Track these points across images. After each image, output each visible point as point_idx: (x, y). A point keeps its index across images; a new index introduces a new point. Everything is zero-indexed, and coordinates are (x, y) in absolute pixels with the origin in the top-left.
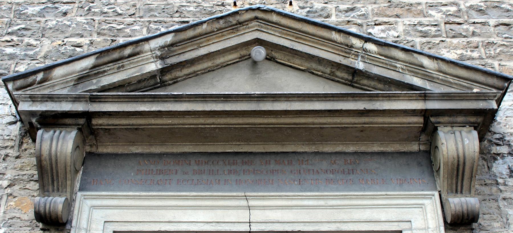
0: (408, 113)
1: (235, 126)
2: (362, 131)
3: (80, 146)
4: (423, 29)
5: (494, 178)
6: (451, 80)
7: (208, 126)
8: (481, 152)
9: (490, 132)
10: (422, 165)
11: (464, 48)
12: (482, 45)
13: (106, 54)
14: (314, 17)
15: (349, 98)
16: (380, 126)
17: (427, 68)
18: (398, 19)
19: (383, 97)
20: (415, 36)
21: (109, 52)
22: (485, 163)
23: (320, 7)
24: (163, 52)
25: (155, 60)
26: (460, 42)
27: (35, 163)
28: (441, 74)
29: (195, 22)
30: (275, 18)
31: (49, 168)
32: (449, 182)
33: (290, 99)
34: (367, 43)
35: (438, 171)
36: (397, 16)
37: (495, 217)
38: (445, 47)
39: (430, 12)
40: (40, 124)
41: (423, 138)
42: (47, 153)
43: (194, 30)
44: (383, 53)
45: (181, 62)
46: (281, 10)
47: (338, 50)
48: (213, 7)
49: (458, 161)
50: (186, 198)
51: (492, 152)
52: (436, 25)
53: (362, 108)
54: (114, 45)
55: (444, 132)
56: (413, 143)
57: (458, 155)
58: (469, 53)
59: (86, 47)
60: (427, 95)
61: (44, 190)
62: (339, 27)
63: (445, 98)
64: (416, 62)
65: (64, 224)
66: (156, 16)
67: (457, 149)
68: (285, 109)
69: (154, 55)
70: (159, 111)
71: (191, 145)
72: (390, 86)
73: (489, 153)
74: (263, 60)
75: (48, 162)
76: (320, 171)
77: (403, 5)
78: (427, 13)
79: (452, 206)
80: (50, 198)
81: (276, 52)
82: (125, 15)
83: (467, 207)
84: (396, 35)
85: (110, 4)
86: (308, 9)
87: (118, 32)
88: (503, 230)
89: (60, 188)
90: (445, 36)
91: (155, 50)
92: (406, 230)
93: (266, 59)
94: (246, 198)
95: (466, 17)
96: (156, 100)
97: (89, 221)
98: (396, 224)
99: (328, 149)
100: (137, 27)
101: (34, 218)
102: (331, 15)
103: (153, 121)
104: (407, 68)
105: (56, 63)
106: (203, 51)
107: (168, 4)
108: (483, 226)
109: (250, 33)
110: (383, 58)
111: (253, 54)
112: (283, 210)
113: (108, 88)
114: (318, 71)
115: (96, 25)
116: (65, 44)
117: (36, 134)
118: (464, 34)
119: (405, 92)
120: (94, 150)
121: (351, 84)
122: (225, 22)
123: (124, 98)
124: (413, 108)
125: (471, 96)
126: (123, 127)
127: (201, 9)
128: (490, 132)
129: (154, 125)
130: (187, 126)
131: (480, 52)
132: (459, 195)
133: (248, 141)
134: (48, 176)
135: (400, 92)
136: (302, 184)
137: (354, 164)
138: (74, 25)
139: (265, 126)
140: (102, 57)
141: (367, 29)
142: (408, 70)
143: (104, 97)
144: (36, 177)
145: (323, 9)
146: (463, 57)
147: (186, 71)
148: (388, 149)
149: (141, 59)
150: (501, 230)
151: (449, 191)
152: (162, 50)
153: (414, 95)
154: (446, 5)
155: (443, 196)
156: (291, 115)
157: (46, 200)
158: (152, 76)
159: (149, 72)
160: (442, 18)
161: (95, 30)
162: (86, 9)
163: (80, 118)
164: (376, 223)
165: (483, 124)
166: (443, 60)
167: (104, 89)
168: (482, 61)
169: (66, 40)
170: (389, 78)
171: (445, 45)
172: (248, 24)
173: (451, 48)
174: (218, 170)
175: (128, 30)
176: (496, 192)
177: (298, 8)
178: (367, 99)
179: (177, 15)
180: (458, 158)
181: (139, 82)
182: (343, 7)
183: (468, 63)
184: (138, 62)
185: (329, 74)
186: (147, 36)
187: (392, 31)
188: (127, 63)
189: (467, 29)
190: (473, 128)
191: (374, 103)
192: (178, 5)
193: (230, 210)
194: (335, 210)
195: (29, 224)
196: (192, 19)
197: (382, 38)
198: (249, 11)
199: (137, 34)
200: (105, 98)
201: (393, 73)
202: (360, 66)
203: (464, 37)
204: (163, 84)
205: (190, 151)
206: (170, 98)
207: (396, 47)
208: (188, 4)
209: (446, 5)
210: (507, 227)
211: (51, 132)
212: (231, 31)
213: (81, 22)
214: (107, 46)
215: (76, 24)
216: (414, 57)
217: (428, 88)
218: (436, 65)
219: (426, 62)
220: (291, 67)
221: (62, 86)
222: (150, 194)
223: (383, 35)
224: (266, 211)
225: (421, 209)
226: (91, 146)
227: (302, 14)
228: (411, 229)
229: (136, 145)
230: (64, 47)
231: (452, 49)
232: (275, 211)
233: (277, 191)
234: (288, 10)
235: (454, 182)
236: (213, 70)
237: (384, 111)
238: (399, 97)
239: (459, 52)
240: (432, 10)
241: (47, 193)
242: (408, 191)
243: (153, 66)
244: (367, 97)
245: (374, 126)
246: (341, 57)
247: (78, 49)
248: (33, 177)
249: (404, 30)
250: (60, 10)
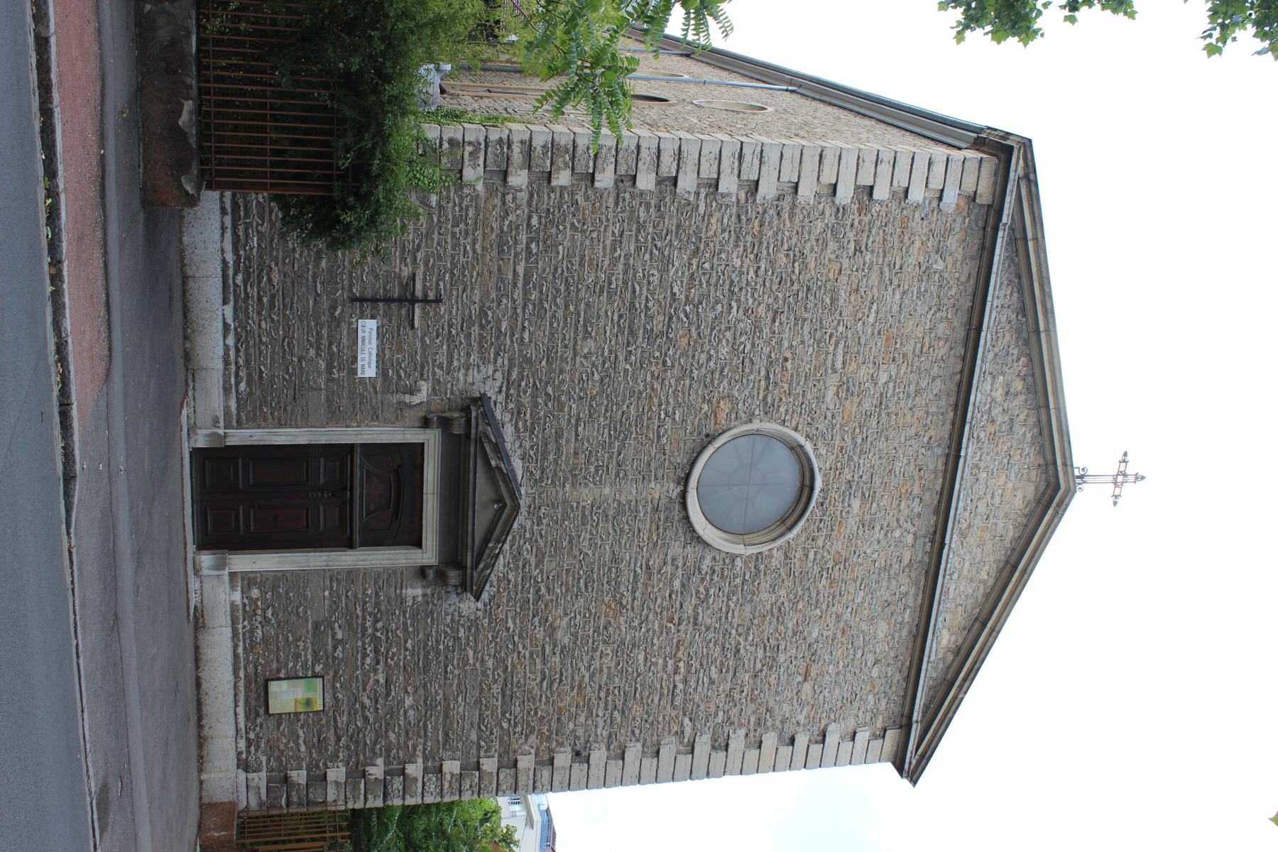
243: (493, 463)
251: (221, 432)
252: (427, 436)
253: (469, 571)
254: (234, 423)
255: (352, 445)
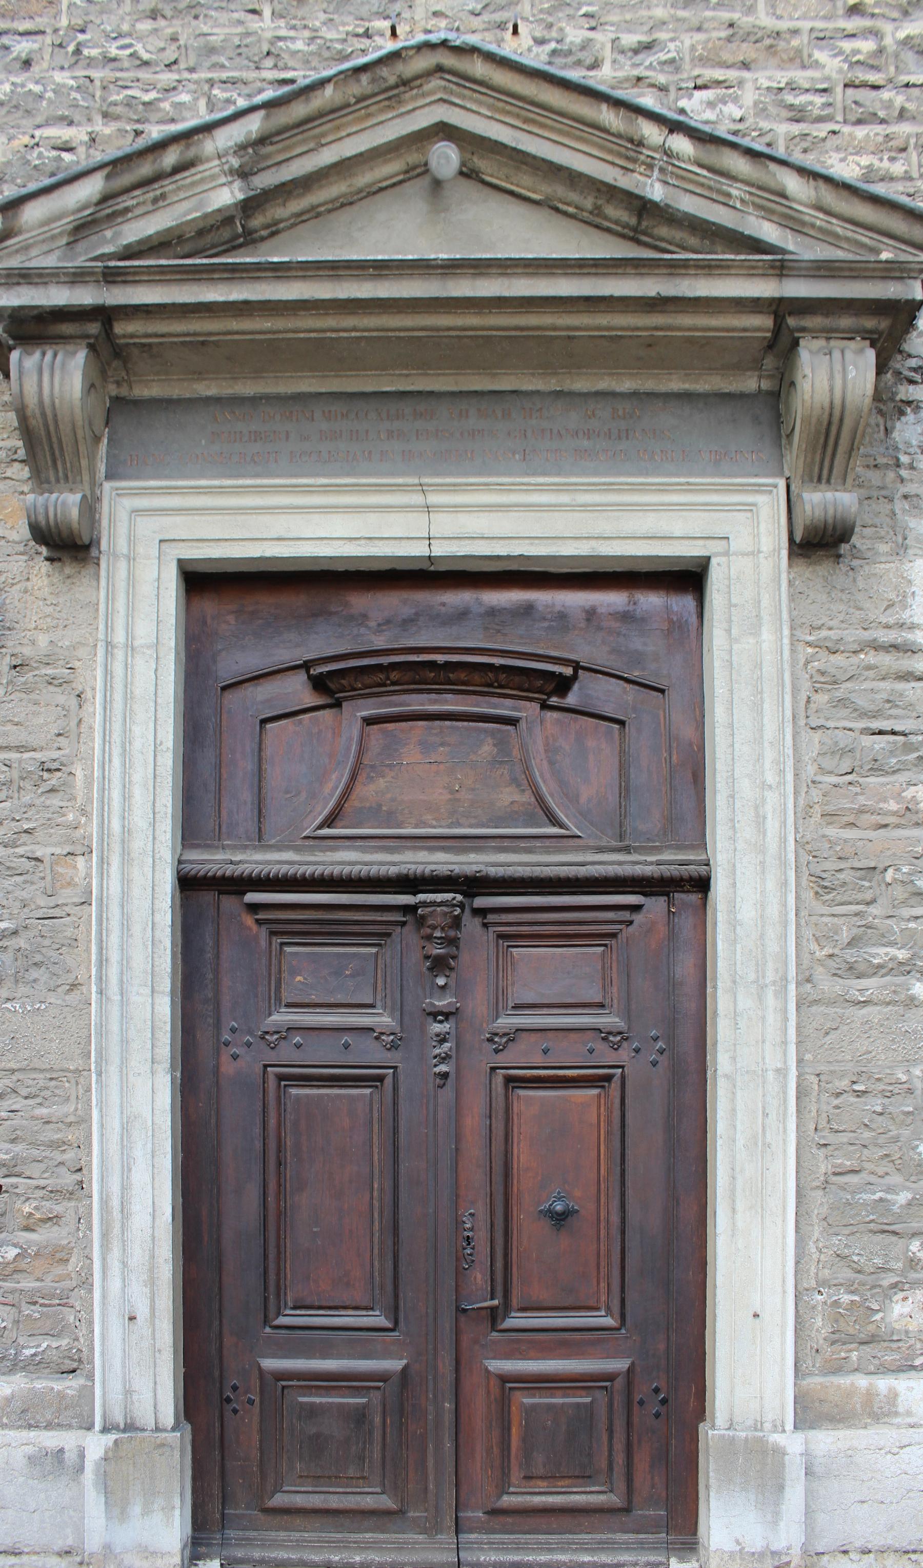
0: (745, 306)
1: (397, 334)
2: (650, 346)
3: (97, 384)
4: (797, 101)
5: (894, 454)
6: (839, 230)
7: (345, 335)
8: (878, 396)
9: (900, 352)
10: (760, 423)
11: (877, 151)
12: (916, 144)
13: (125, 165)
14: (564, 67)
15: (629, 270)
16: (686, 334)
17: (794, 200)
18: (746, 74)
19: (697, 267)
20: (777, 119)
21: (131, 160)
22: (881, 421)
23: (578, 40)
24: (243, 160)
25: (230, 179)
26: (872, 134)
27: (16, 424)
28: (821, 216)
29: (307, 81)
30: (479, 68)
31: (43, 433)
32: (809, 460)
33: (509, 271)
34: (675, 135)
35: (790, 436)
36: (745, 65)
37: (883, 533)
38: (838, 149)
39: (818, 55)
40: (14, 338)
41: (769, 362)
42: (36, 400)
43: (308, 100)
44: (706, 161)
45: (283, 184)
46: (493, 48)
47: (610, 151)
48: (345, 40)
49: (831, 415)
50: (308, 490)
51: (898, 398)
52: (824, 90)
53: (653, 294)
54: (141, 143)
55: (811, 352)
56: (749, 373)
57: (832, 403)
58: (886, 164)
59: (82, 150)
60: (785, 264)
61: (41, 479)
62: (619, 94)
63: (822, 273)
64: (772, 185)
65: (87, 548)
66: (223, 66)
67: (831, 390)
68: (498, 294)
69: (226, 167)
70: (246, 302)
71: (313, 377)
72: (713, 243)
73: (892, 400)
74: (455, 178)
75: (40, 420)
76: (563, 432)
77: (760, 35)
78: (810, 56)
79: (808, 508)
80: (54, 496)
81: (482, 157)
82: (157, 64)
83: (835, 511)
84: (738, 114)
85: (120, 36)
86: (553, 45)
87: (146, 111)
88: (894, 558)
89: (69, 474)
90: (840, 118)
91: (226, 154)
92: (717, 554)
93: (461, 173)
94: (422, 489)
95: (892, 69)
96: (238, 275)
97: (132, 540)
98: (701, 542)
99: (581, 385)
100: (185, 98)
101: (30, 536)
102: (602, 61)
103: (235, 324)
104: (752, 198)
105: (24, 191)
106: (327, 156)
107: (248, 34)
108: (859, 551)
109: (427, 109)
110: (704, 172)
111: (433, 164)
112: (492, 514)
113: (136, 249)
114: (568, 204)
115: (98, 94)
116: (37, 145)
117: (8, 359)
118: (881, 114)
119: (743, 257)
120: (124, 392)
121: (634, 236)
122: (373, 81)
123: (172, 272)
124: (756, 295)
125: (874, 270)
126: (176, 340)
127: (320, 47)
128: (900, 352)
129: (237, 333)
130: (302, 335)
131: (908, 161)
132: (823, 486)
133: (424, 367)
134: (43, 449)
135: (732, 257)
136: (529, 460)
137: (631, 417)
138: (49, 95)
139: (458, 333)
140: (117, 174)
141: (677, 100)
142: (753, 204)
143: (132, 270)
144: (22, 454)
145: (585, 45)
146: (872, 175)
147: (296, 206)
148: (698, 387)
149: (199, 176)
150: (890, 558)
151: (806, 478)
152: (242, 153)
153: (760, 264)
154: (853, 36)
155: (793, 488)
156: (509, 307)
157: (47, 500)
158: (225, 218)
159: (219, 210)
160: (840, 71)
161: (97, 106)
162: (71, 48)
163: (91, 321)
164: (663, 542)
165: (890, 334)
166: (828, 180)
167: (130, 253)
168: (909, 184)
169: (37, 133)
170: (714, 224)
171: (839, 142)
172: (421, 85)
173: (851, 150)
174: (367, 432)
175: (166, 105)
176: (893, 482)
177: (531, 43)
178: (665, 271)
179: (269, 62)
180: (832, 407)
181: (201, 233)
182: (630, 39)
183: (880, 189)
184: (193, 184)
185: (591, 213)
186: (209, 118)
187: (730, 104)
188: (170, 187)
189: (890, 100)
190: (868, 342)
191: (678, 281)
192: (269, 35)
193: (392, 515)
194: (588, 514)
195: (22, 549)
196: (302, 73)
197: (707, 122)
198: (424, 50)
199: (187, 114)
200: (135, 274)
201: (722, 210)
202: (656, 192)
203: (881, 123)
204: (250, 239)
205: (312, 390)
206: (266, 270)
207: (734, 146)
208: (292, 33)
209: (853, 36)
210: (902, 552)
211: (37, 355)
212: (387, 103)
213: (64, 86)
214: (127, 145)
215: (54, 91)
216: (768, 172)
217: (791, 247)
218: (813, 193)
219: (792, 183)
220: (512, 193)
221: (45, 248)
222: (240, 482)
223: (710, 115)
224: (459, 515)
225: (749, 515)
226: (118, 383)
227: (537, 58)
228: (727, 554)
229: (205, 379)
230: (36, 151)
231: (851, 154)
232: (476, 514)
233: (479, 474)
234: (509, 48)
235: (818, 459)
236: (351, 203)
237: (697, 300)
238: (728, 267)
239: (865, 161)
240: (821, 49)
241: (46, 486)
242: (730, 476)
243: (226, 196)
244: (666, 266)
245: (674, 334)
246: (618, 170)
247: (67, 157)
248: (16, 452)
249: (756, 104)
250: (15, 55)
251: (96, 1445)
252: (148, 550)
253: (797, 289)
254: (70, 1385)
255: (189, 884)
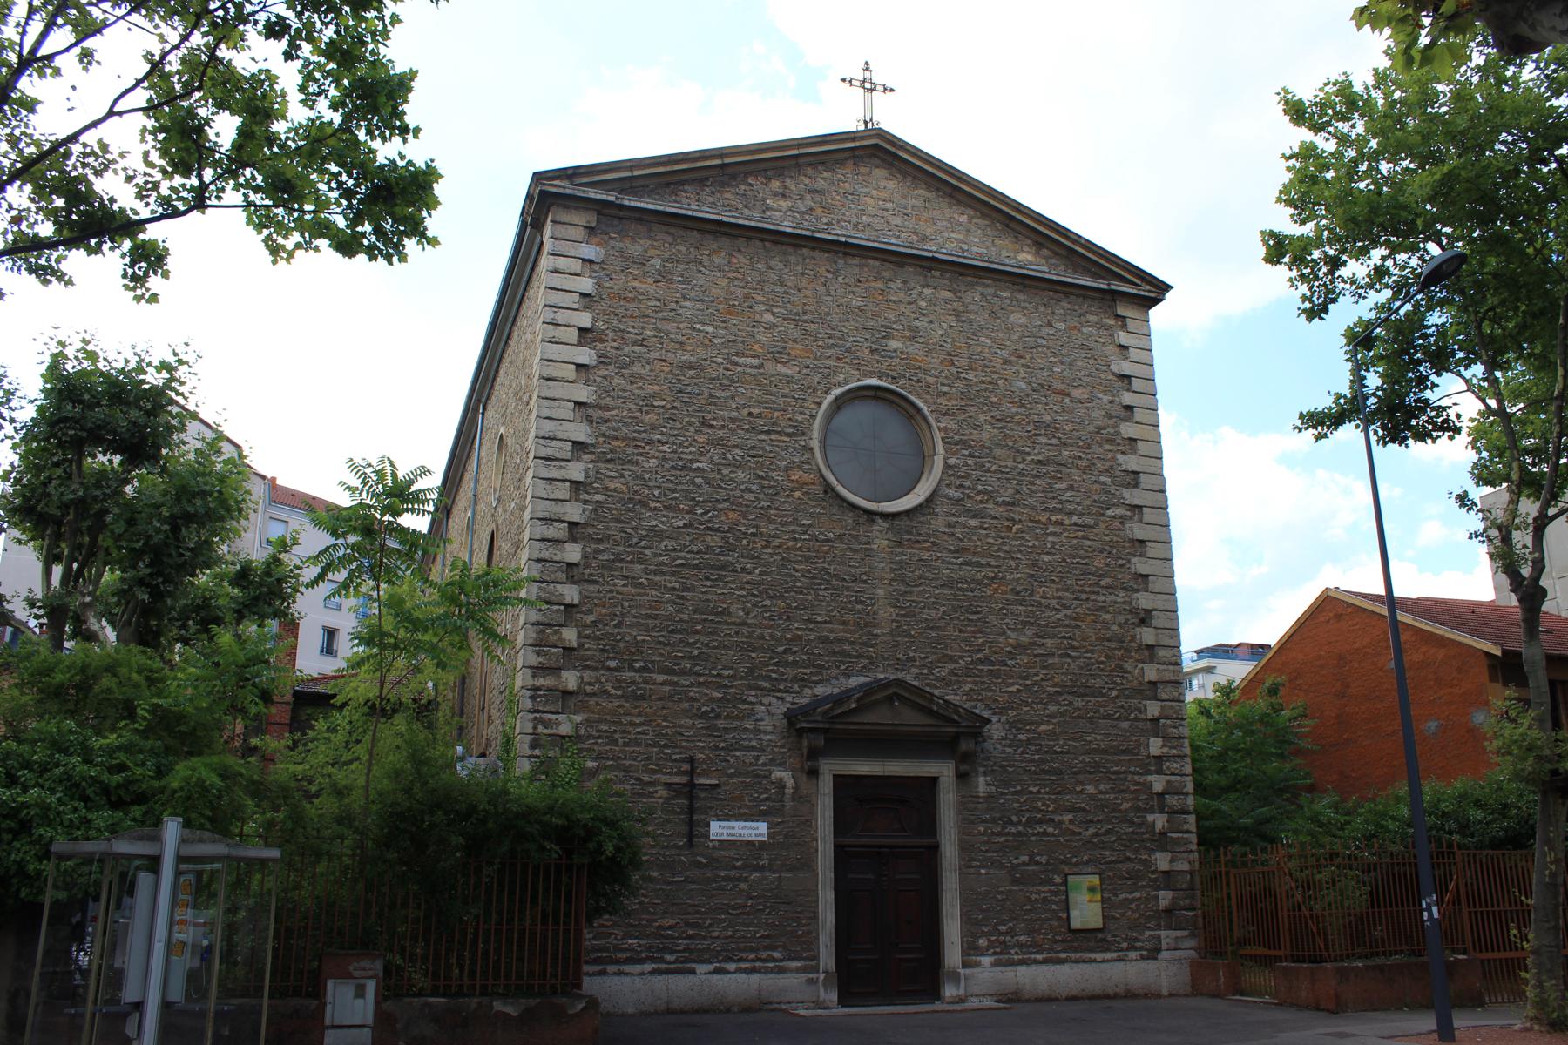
251: (822, 976)
